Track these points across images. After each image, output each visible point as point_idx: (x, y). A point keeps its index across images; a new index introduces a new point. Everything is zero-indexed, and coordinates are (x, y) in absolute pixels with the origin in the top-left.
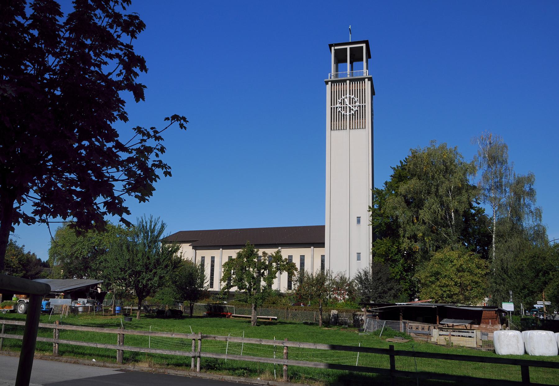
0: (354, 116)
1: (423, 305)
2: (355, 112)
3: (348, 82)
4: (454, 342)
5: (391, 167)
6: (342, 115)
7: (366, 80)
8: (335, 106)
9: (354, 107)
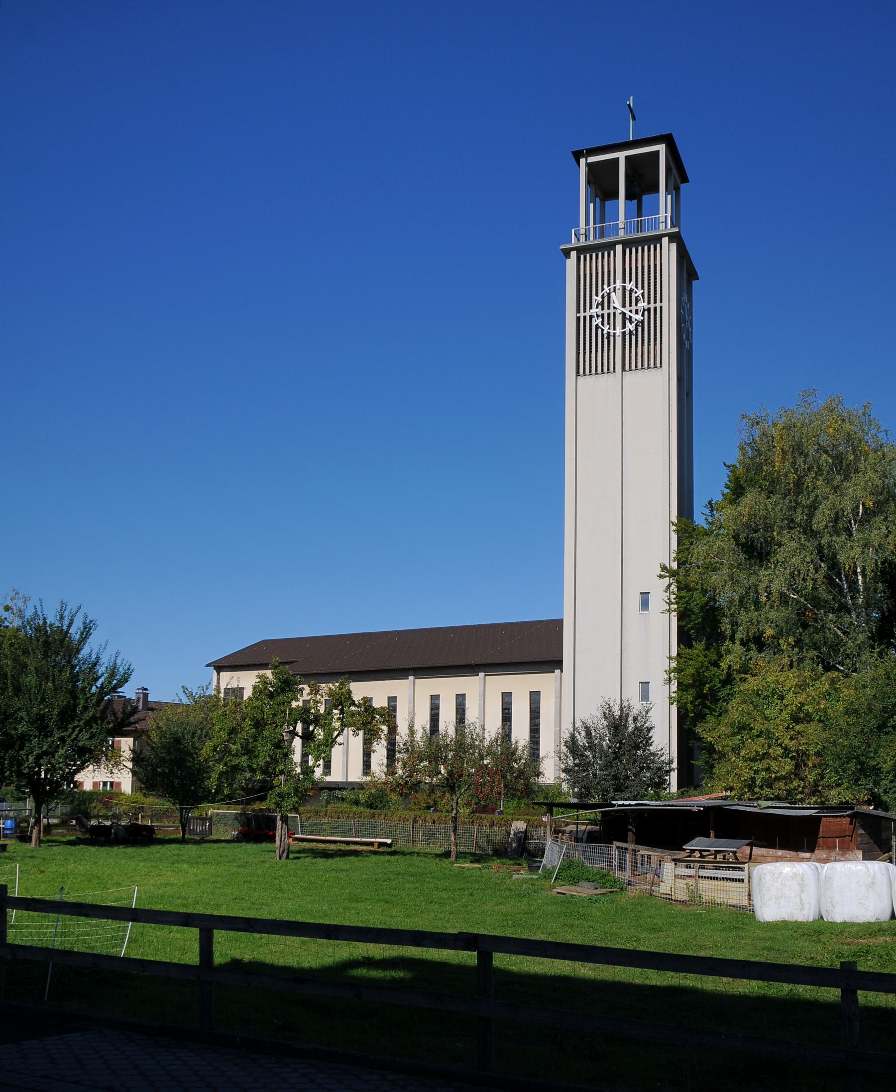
0: (634, 337)
1: (673, 806)
2: (637, 326)
3: (619, 248)
4: (703, 893)
5: (725, 464)
6: (606, 336)
7: (665, 240)
8: (588, 314)
9: (634, 311)
